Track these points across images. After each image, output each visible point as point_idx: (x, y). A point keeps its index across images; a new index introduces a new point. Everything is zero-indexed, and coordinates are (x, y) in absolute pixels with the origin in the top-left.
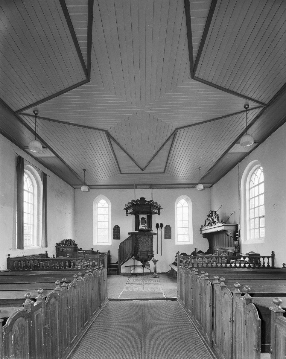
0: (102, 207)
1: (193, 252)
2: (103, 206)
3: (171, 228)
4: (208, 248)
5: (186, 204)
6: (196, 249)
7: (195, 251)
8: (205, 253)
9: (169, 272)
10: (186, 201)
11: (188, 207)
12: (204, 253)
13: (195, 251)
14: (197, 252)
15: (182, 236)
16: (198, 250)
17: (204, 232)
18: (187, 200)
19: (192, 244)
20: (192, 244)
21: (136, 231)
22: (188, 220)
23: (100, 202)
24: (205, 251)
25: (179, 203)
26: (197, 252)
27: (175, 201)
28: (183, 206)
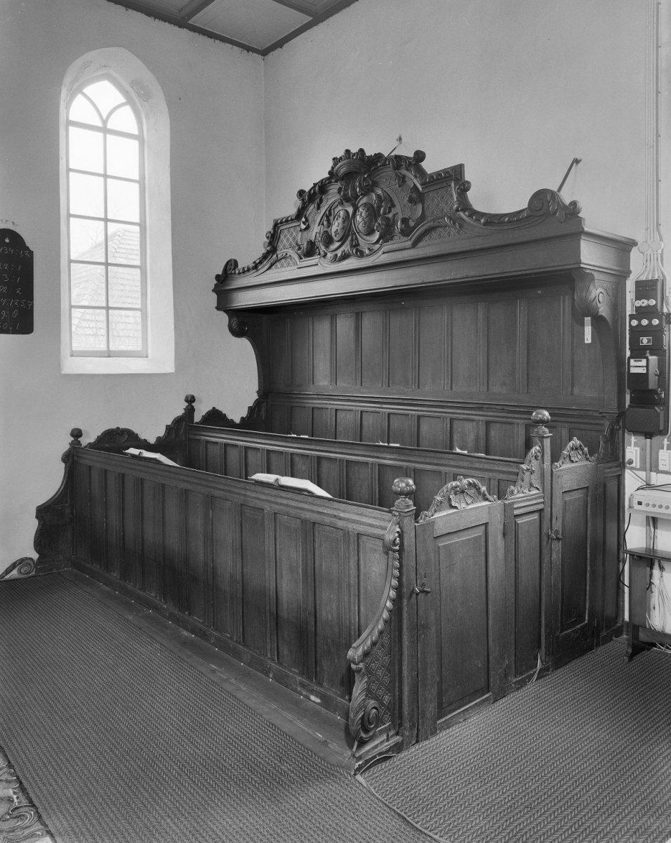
0: (100, 124)
1: (178, 421)
2: (105, 122)
3: (31, 253)
4: (256, 397)
5: (126, 119)
6: (191, 400)
7: (190, 411)
8: (237, 420)
9: (14, 573)
10: (130, 101)
11: (140, 138)
12: (231, 424)
13: (190, 411)
14: (198, 418)
15: (103, 318)
16: (201, 411)
17: (246, 300)
18: (136, 95)
19: (169, 367)
20: (169, 367)
21: (639, 284)
22: (137, 220)
23: (88, 90)
24: (237, 413)
25: (80, 97)
26: (198, 418)
27: (61, 77)
28: (109, 126)
